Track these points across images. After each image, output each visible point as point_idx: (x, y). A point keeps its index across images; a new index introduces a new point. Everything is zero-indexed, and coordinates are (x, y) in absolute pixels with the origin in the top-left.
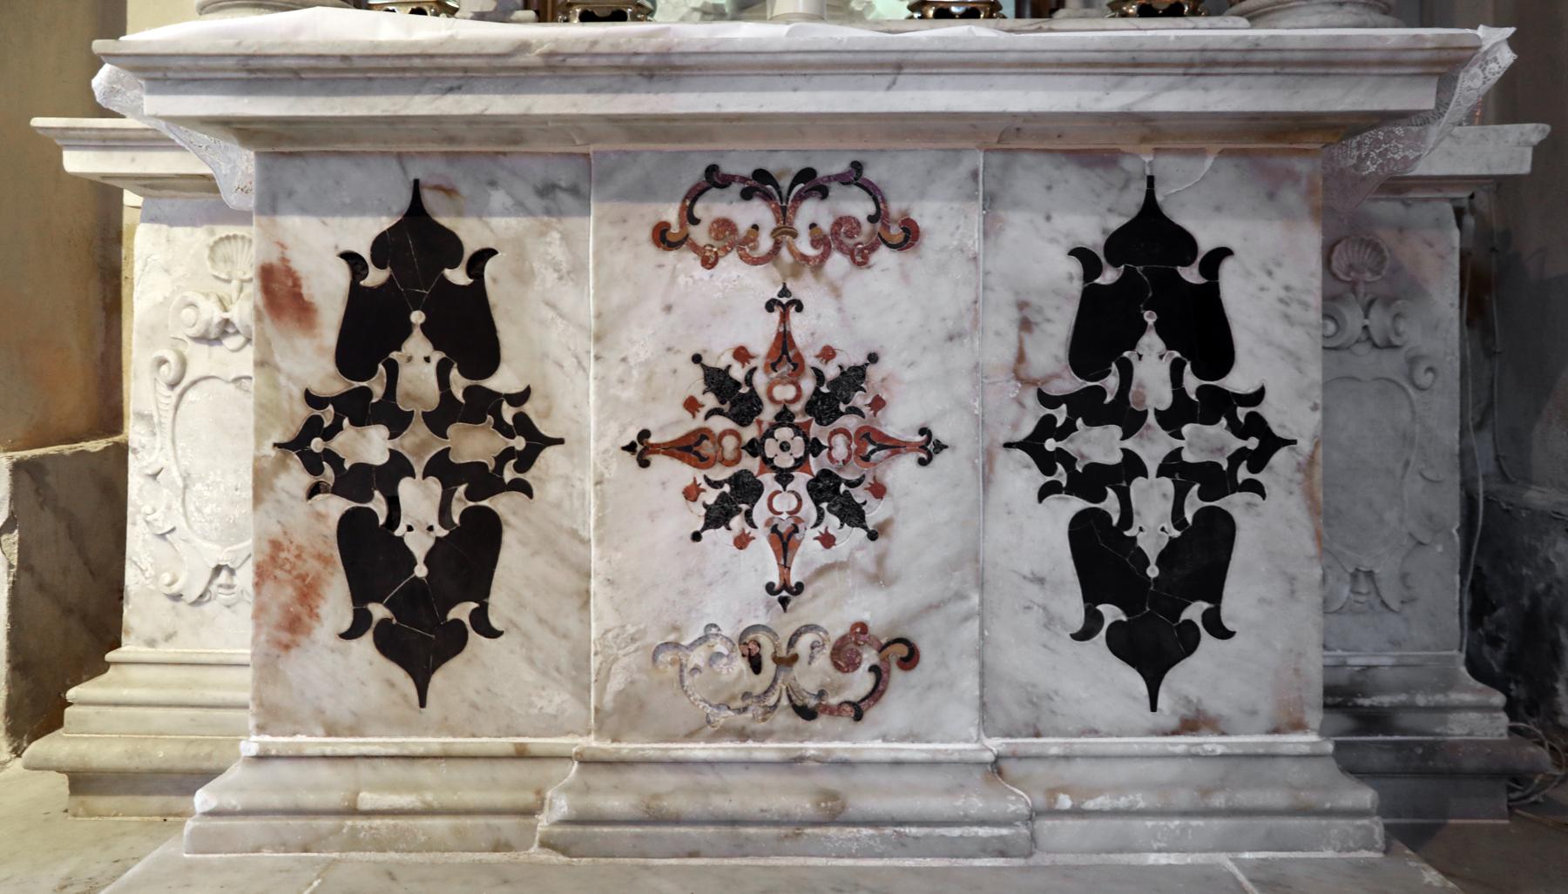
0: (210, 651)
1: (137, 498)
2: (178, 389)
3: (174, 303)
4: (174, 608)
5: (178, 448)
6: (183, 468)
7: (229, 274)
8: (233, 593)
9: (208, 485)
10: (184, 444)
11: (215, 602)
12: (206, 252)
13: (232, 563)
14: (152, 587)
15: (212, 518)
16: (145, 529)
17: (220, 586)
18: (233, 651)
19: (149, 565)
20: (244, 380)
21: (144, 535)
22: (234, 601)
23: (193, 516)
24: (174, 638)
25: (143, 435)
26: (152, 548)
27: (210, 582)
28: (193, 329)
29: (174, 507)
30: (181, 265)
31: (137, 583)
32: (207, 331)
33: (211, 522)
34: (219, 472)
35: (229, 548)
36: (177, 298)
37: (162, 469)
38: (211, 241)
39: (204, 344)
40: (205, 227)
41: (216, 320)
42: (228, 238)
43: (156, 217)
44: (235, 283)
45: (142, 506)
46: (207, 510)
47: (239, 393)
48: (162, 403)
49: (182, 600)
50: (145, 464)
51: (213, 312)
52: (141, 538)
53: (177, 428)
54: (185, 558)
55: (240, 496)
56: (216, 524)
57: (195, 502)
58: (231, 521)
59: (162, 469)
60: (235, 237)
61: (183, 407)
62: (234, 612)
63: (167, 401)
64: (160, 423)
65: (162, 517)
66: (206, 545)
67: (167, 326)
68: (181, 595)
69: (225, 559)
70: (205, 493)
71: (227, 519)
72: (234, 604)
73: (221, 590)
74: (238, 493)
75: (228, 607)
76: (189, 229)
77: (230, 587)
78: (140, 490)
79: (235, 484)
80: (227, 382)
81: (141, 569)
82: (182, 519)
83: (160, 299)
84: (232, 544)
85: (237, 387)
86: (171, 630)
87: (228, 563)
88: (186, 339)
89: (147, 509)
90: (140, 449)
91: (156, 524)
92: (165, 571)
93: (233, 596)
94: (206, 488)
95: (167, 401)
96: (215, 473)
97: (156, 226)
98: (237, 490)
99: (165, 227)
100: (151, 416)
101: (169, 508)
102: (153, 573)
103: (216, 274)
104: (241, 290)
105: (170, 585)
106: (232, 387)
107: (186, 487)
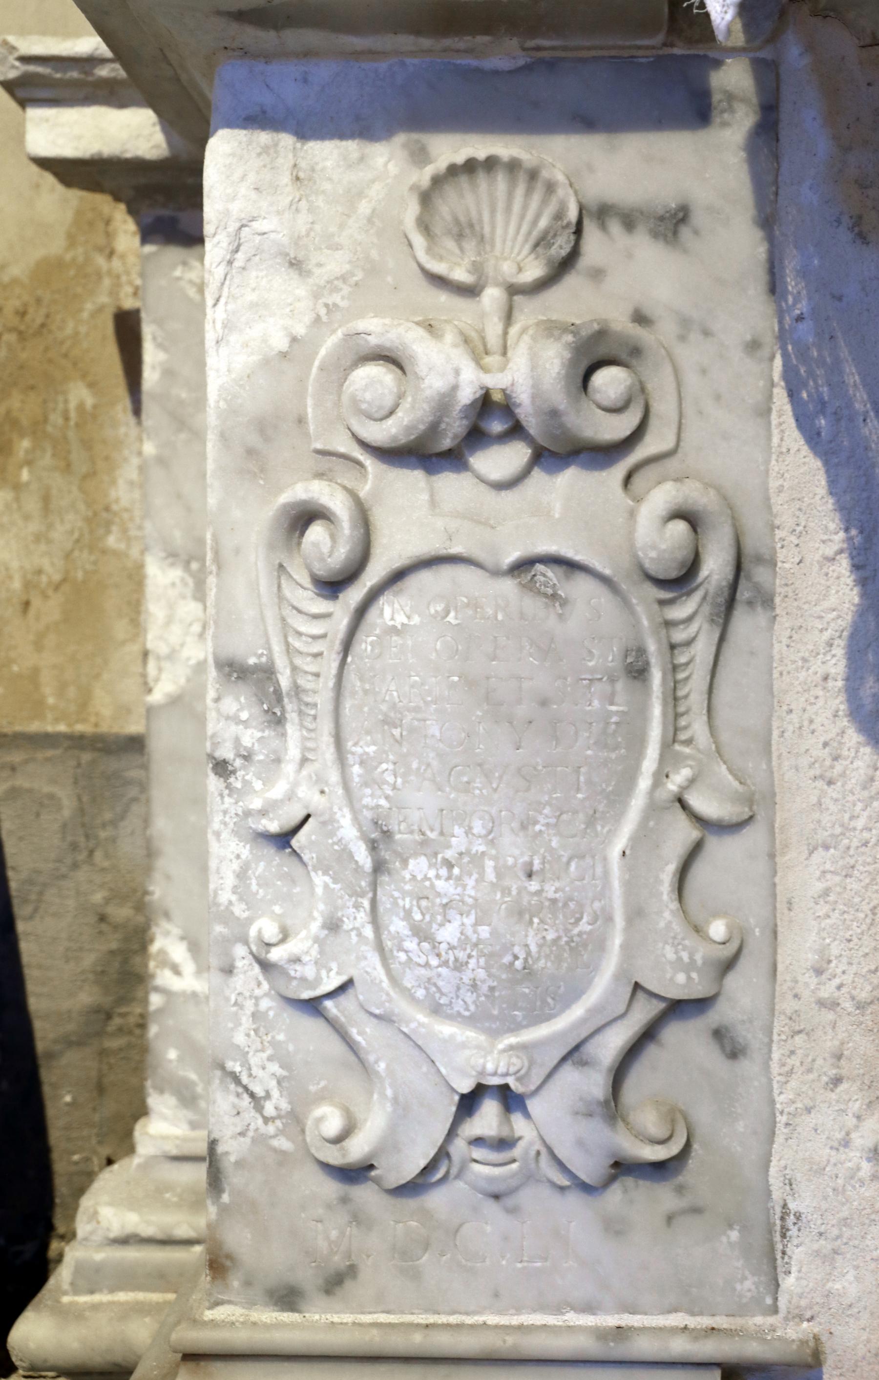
0: (453, 1319)
1: (234, 898)
2: (355, 595)
3: (323, 352)
4: (344, 1200)
5: (351, 759)
6: (368, 814)
7: (477, 268)
8: (514, 1161)
9: (450, 865)
10: (371, 749)
11: (460, 1184)
12: (412, 209)
13: (519, 1080)
14: (283, 1144)
15: (462, 955)
16: (259, 984)
17: (478, 1141)
18: (515, 1320)
19: (274, 1083)
20: (540, 567)
21: (257, 999)
22: (513, 1183)
23: (401, 949)
24: (348, 1284)
25: (246, 723)
26: (281, 1037)
27: (452, 1133)
28: (390, 422)
29: (347, 925)
30: (337, 247)
31: (242, 1134)
32: (434, 429)
33: (459, 966)
34: (478, 827)
35: (512, 1040)
36: (330, 343)
37: (308, 816)
38: (424, 176)
39: (413, 467)
40: (400, 138)
41: (467, 395)
42: (470, 167)
43: (264, 112)
44: (492, 296)
45: (250, 921)
46: (448, 934)
47: (532, 605)
48: (299, 634)
49: (367, 1179)
50: (256, 804)
51: (457, 372)
52: (249, 1006)
53: (348, 705)
54: (382, 1066)
55: (539, 893)
56: (476, 969)
57: (408, 914)
58: (518, 964)
59: (308, 816)
60: (491, 163)
61: (365, 644)
62: (513, 1211)
63: (316, 628)
64: (297, 690)
65: (315, 951)
66: (446, 1029)
67: (301, 421)
68: (371, 1167)
69: (502, 1069)
70: (441, 885)
71: (507, 959)
72: (513, 1191)
73: (478, 1153)
74: (534, 886)
75: (496, 1197)
76: (352, 147)
77: (503, 1143)
78: (242, 875)
79: (526, 858)
80: (496, 573)
81: (252, 1095)
82: (374, 959)
83: (280, 343)
84: (515, 1027)
85: (523, 586)
86: (338, 1261)
87: (511, 1081)
88: (358, 454)
89: (269, 929)
90: (238, 763)
91: (296, 970)
92: (322, 1097)
93: (514, 1166)
94: (444, 872)
95: (316, 628)
96: (469, 831)
97: (264, 137)
98: (530, 875)
99: (287, 140)
100: (268, 672)
101: (333, 926)
102: (285, 1106)
103: (438, 267)
104: (509, 318)
105: (338, 1140)
106: (508, 586)
107: (379, 867)
